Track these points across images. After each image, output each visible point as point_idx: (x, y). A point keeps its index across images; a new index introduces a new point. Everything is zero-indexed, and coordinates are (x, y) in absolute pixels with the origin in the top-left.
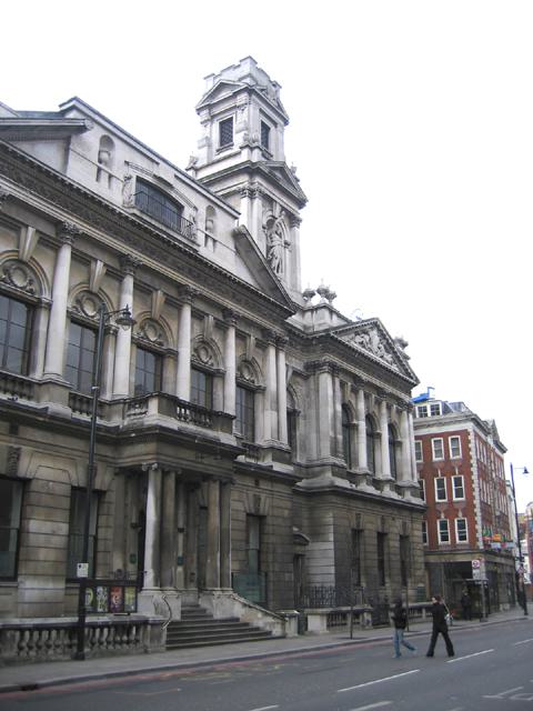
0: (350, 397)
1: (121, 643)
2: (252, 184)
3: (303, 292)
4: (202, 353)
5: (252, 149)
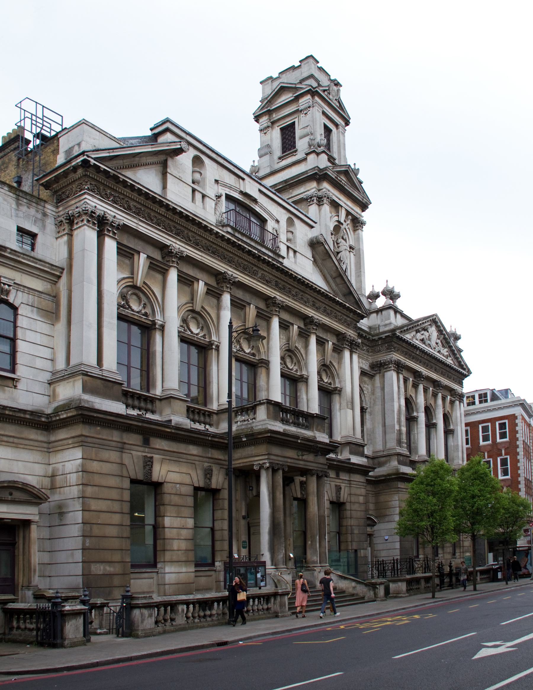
0: (411, 392)
1: (205, 616)
2: (319, 190)
3: (367, 294)
4: (288, 361)
5: (318, 154)
